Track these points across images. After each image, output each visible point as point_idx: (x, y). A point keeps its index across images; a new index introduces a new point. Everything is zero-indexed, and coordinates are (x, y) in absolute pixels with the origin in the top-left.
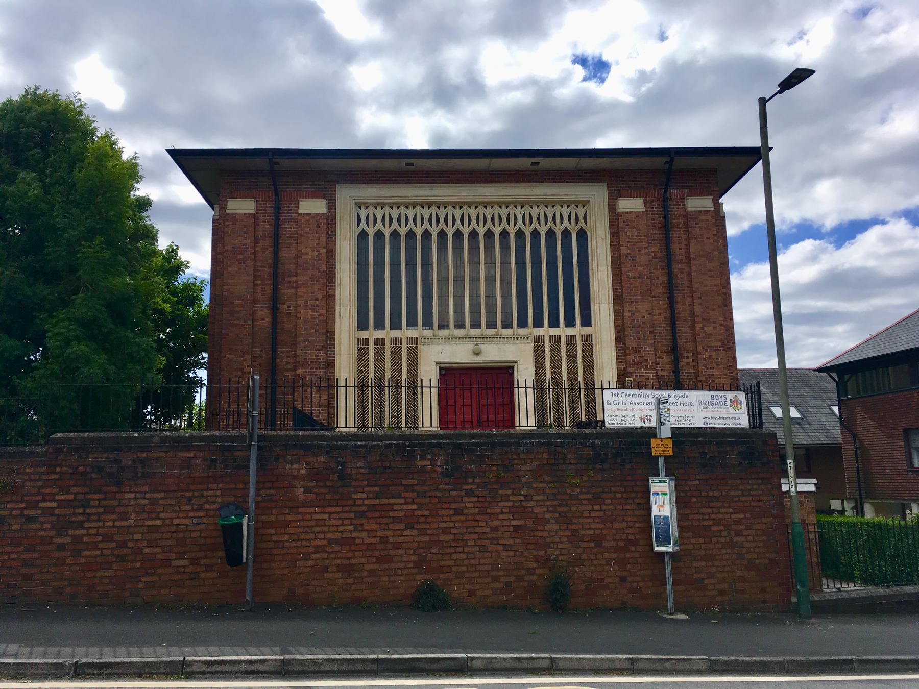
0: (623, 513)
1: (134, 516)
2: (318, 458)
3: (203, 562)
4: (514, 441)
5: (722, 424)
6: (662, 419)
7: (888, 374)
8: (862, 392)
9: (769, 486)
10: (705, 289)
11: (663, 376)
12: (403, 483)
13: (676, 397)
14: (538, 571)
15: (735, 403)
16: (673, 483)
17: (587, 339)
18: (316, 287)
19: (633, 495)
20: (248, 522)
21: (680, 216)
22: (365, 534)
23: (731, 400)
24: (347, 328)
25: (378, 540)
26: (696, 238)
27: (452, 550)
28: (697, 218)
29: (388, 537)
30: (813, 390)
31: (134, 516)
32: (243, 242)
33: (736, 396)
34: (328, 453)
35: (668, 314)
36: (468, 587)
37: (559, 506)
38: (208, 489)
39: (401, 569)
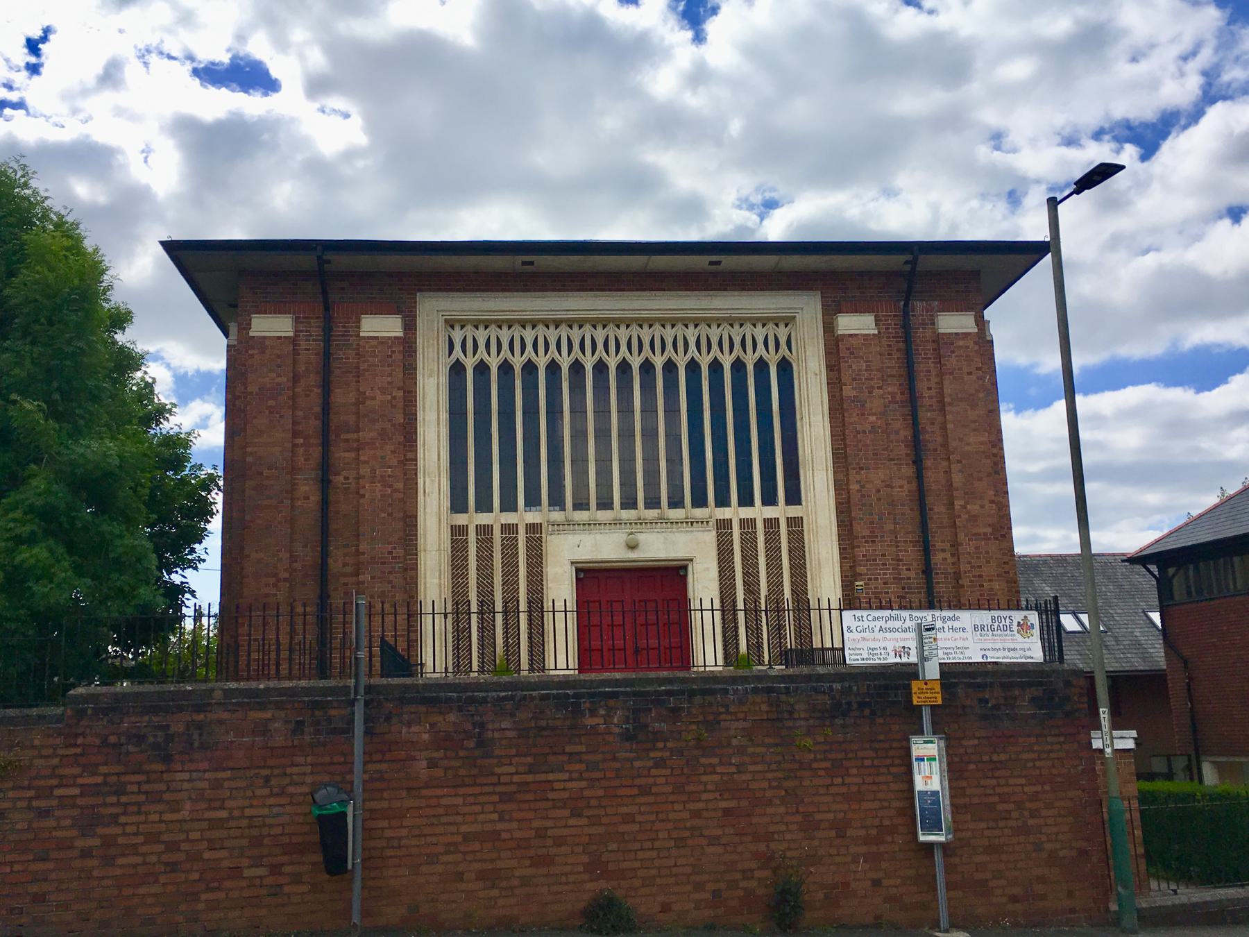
0: (875, 788)
1: (188, 806)
2: (447, 716)
3: (287, 869)
4: (720, 686)
5: (1007, 658)
6: (926, 653)
7: (1233, 566)
8: (1194, 594)
9: (1075, 746)
10: (967, 448)
11: (909, 578)
12: (567, 750)
13: (944, 620)
14: (758, 874)
15: (1024, 627)
16: (942, 744)
17: (796, 525)
18: (389, 447)
19: (889, 761)
20: (354, 810)
21: (928, 341)
22: (514, 825)
23: (1019, 623)
24: (435, 509)
25: (533, 833)
26: (951, 374)
27: (637, 846)
28: (952, 343)
29: (547, 828)
30: (1121, 587)
31: (188, 806)
32: (276, 381)
33: (1026, 617)
34: (460, 709)
35: (914, 486)
36: (661, 899)
37: (784, 778)
38: (293, 765)
39: (566, 874)
